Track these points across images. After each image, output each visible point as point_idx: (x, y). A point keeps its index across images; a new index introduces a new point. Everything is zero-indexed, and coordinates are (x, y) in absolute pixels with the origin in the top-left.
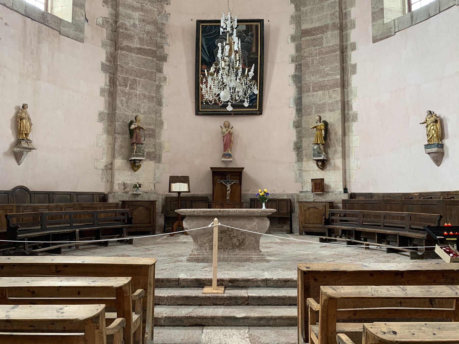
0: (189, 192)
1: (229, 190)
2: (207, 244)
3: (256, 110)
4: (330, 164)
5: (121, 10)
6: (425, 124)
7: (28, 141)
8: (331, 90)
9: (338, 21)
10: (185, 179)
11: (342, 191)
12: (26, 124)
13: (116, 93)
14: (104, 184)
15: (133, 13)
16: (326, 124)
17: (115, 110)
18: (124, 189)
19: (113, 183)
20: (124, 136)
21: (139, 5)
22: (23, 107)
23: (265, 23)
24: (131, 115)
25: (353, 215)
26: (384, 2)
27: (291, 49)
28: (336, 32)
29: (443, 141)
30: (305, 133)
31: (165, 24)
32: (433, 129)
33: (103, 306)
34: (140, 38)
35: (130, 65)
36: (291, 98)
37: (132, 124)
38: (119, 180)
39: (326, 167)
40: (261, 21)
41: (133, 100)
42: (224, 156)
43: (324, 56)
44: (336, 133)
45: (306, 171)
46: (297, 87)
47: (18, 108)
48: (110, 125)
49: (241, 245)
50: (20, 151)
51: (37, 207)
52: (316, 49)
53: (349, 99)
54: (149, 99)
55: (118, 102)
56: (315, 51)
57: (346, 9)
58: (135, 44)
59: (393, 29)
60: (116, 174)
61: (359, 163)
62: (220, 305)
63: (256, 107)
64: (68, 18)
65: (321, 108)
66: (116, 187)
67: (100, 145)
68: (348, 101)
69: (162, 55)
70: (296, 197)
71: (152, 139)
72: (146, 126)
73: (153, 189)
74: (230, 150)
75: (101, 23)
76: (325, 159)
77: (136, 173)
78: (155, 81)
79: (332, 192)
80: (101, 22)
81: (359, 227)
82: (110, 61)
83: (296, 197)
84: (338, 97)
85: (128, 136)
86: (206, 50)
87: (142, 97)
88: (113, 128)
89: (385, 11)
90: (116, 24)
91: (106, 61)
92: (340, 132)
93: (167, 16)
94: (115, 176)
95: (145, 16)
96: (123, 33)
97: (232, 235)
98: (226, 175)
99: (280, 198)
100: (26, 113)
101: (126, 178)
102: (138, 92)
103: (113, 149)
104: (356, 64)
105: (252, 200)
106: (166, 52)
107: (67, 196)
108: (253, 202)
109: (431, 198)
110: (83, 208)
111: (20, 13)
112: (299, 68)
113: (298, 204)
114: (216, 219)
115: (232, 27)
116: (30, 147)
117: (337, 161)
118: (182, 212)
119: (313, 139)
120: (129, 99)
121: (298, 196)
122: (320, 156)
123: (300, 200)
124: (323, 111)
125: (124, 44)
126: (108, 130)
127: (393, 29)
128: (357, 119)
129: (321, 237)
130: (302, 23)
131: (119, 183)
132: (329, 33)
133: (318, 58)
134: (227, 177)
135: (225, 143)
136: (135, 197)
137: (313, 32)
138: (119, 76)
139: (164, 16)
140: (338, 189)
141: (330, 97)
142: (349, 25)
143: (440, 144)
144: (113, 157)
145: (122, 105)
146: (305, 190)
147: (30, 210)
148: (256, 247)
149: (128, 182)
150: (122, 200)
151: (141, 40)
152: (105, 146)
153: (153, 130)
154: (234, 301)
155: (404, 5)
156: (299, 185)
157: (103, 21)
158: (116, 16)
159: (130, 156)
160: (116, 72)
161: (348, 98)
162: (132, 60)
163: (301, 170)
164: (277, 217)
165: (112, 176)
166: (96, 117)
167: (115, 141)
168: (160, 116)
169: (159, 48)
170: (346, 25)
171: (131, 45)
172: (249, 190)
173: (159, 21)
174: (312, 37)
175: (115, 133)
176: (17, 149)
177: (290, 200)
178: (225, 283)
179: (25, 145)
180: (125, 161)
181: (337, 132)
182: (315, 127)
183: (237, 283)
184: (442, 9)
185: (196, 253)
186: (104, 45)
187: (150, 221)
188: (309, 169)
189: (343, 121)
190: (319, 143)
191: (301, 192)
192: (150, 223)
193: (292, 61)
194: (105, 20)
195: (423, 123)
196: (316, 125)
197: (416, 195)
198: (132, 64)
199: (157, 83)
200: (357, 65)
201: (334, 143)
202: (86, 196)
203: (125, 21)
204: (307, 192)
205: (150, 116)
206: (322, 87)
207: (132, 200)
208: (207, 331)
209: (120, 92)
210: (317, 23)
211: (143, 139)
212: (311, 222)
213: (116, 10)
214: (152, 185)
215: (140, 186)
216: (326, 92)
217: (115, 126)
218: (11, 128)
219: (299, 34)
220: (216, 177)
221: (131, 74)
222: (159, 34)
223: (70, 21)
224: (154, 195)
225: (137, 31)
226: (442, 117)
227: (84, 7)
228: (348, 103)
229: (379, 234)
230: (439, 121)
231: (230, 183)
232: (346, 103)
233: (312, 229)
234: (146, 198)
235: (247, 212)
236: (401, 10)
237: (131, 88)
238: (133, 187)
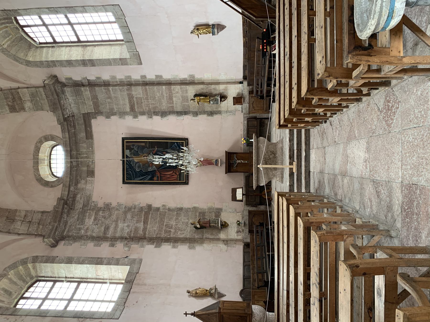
0: (242, 188)
2: (273, 172)
4: (223, 92)
5: (118, 235)
6: (199, 35)
7: (211, 289)
9: (125, 87)
10: (234, 191)
12: (200, 291)
13: (176, 238)
14: (237, 246)
15: (120, 227)
16: (196, 96)
17: (187, 238)
18: (240, 232)
19: (236, 239)
20: (204, 232)
21: (114, 223)
22: (189, 293)
23: (124, 136)
24: (190, 228)
25: (258, 80)
27: (143, 119)
28: (133, 88)
29: (210, 24)
30: (201, 109)
32: (203, 31)
33: (299, 218)
34: (137, 223)
36: (177, 118)
37: (197, 227)
38: (235, 235)
39: (225, 95)
40: (123, 139)
42: (217, 164)
43: (149, 97)
44: (202, 89)
45: (228, 109)
46: (169, 114)
47: (190, 296)
48: (197, 242)
49: (274, 153)
50: (217, 294)
51: (253, 279)
52: (144, 102)
54: (178, 216)
55: (182, 236)
56: (145, 102)
57: (117, 82)
58: (141, 225)
59: (135, 53)
61: (223, 74)
62: (301, 164)
63: (183, 143)
64: (127, 268)
65: (185, 99)
66: (240, 237)
67: (211, 248)
68: (181, 81)
69: (147, 208)
70: (246, 115)
71: (206, 214)
73: (241, 213)
74: (213, 161)
76: (220, 96)
77: (229, 225)
78: (166, 212)
79: (242, 91)
80: (127, 248)
81: (265, 78)
82: (154, 242)
83: (246, 115)
84: (177, 88)
85: (204, 230)
86: (143, 177)
88: (199, 239)
89: (122, 57)
90: (128, 239)
91: (153, 245)
92: (202, 86)
93: (119, 205)
94: (232, 238)
95: (121, 220)
96: (134, 234)
98: (231, 163)
99: (246, 125)
100: (193, 291)
101: (233, 231)
103: (213, 239)
104: (156, 76)
106: (145, 205)
107: (245, 268)
108: (249, 145)
110: (254, 255)
111: (129, 295)
114: (258, 166)
115: (159, 158)
116: (214, 288)
117: (221, 88)
118: (255, 186)
119: (206, 104)
121: (245, 114)
122: (218, 99)
124: (187, 97)
125: (142, 233)
126: (200, 243)
127: (135, 53)
128: (193, 75)
130: (125, 111)
132: (133, 93)
134: (232, 163)
136: (246, 225)
137: (132, 104)
139: (120, 207)
141: (177, 93)
142: (129, 80)
144: (219, 239)
145: (184, 233)
146: (241, 109)
147: (255, 283)
148: (275, 145)
150: (248, 233)
152: (212, 245)
154: (299, 157)
155: (117, 44)
156: (237, 113)
158: (122, 238)
160: (161, 238)
161: (178, 81)
162: (152, 227)
164: (260, 128)
165: (232, 240)
166: (192, 251)
167: (208, 238)
168: (190, 209)
170: (129, 81)
171: (142, 228)
173: (123, 210)
174: (136, 104)
175: (202, 238)
176: (216, 296)
177: (247, 119)
178: (291, 161)
179: (214, 291)
180: (221, 232)
182: (198, 103)
183: (292, 155)
184: (126, 26)
185: (278, 179)
186: (142, 246)
187: (262, 214)
188: (226, 107)
189: (194, 84)
190: (209, 100)
191: (242, 112)
192: (263, 214)
193: (151, 118)
195: (198, 36)
196: (196, 102)
197: (244, 40)
198: (155, 227)
199: (167, 211)
201: (209, 90)
202: (246, 257)
203: (125, 232)
204: (242, 108)
205: (190, 215)
206: (170, 98)
207: (248, 226)
208: (312, 170)
209: (175, 235)
210: (126, 101)
211: (206, 220)
212: (263, 106)
213: (118, 239)
214: (238, 214)
215: (239, 221)
216: (174, 95)
217: (198, 238)
218: (203, 299)
219: (132, 113)
220: (232, 170)
221: (162, 228)
222: (133, 210)
223: (129, 267)
225: (132, 224)
226: (195, 25)
227: (118, 258)
228: (182, 81)
229: (269, 69)
231: (236, 160)
232: (182, 82)
233: (267, 106)
235: (255, 150)
236: (120, 46)
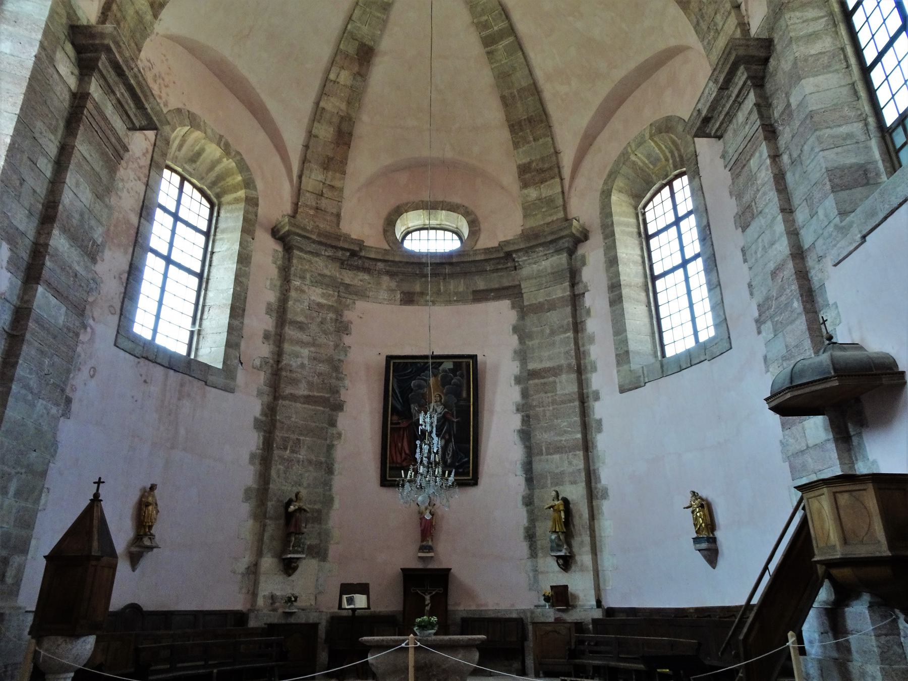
1: (429, 604)
3: (469, 478)
4: (576, 562)
5: (287, 347)
6: (691, 509)
8: (571, 454)
10: (363, 589)
11: (593, 605)
12: (152, 512)
15: (302, 350)
16: (566, 502)
17: (268, 484)
24: (289, 490)
26: (629, 343)
27: (514, 394)
30: (539, 514)
31: (343, 361)
35: (293, 419)
36: (518, 463)
39: (571, 567)
41: (294, 468)
42: (422, 549)
44: (581, 516)
47: (144, 491)
50: (139, 552)
52: (548, 397)
53: (596, 467)
55: (273, 473)
57: (583, 345)
60: (262, 579)
63: (468, 474)
65: (558, 479)
66: (260, 602)
70: (529, 615)
72: (309, 506)
75: (259, 366)
76: (568, 554)
77: (290, 578)
78: (326, 440)
80: (258, 364)
83: (529, 615)
84: (579, 463)
86: (399, 395)
87: (306, 463)
90: (278, 365)
93: (346, 349)
97: (430, 674)
99: (507, 616)
100: (153, 496)
102: (301, 457)
103: (261, 540)
105: (464, 620)
106: (342, 398)
109: (709, 616)
112: (526, 420)
113: (531, 626)
117: (584, 558)
118: (368, 641)
119: (550, 524)
120: (288, 468)
122: (561, 551)
123: (536, 620)
128: (608, 496)
129: (563, 678)
130: (528, 361)
131: (264, 595)
132: (564, 377)
133: (551, 408)
135: (423, 528)
137: (543, 374)
138: (277, 436)
140: (589, 601)
141: (570, 463)
142: (589, 368)
143: (711, 538)
144: (260, 554)
145: (279, 477)
149: (278, 593)
150: (269, 622)
151: (311, 385)
153: (319, 512)
157: (261, 362)
158: (279, 354)
159: (284, 550)
161: (594, 465)
162: (296, 413)
163: (535, 571)
165: (256, 584)
168: (330, 490)
169: (333, 393)
172: (459, 604)
174: (542, 381)
176: (134, 549)
180: (275, 560)
181: (582, 515)
182: (552, 507)
190: (557, 530)
193: (518, 410)
194: (265, 361)
195: (687, 508)
196: (552, 503)
198: (296, 418)
200: (603, 420)
201: (579, 530)
206: (559, 449)
209: (277, 458)
211: (304, 525)
214: (313, 598)
215: (296, 600)
216: (565, 456)
219: (525, 374)
222: (334, 375)
224: (315, 614)
226: (710, 499)
228: (595, 473)
230: (705, 506)
232: (592, 472)
234: (302, 619)
236: (652, 352)
237: (293, 451)
238: (286, 602)
